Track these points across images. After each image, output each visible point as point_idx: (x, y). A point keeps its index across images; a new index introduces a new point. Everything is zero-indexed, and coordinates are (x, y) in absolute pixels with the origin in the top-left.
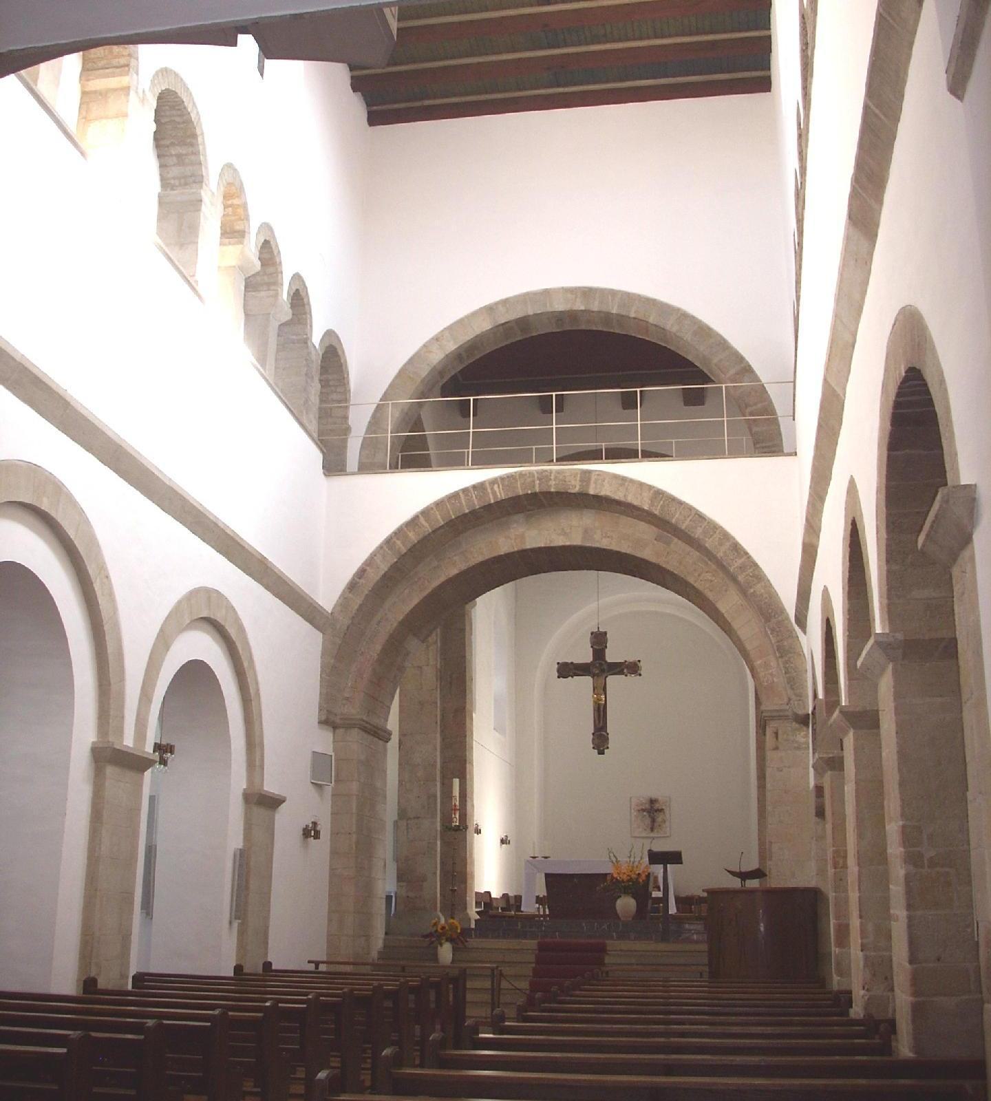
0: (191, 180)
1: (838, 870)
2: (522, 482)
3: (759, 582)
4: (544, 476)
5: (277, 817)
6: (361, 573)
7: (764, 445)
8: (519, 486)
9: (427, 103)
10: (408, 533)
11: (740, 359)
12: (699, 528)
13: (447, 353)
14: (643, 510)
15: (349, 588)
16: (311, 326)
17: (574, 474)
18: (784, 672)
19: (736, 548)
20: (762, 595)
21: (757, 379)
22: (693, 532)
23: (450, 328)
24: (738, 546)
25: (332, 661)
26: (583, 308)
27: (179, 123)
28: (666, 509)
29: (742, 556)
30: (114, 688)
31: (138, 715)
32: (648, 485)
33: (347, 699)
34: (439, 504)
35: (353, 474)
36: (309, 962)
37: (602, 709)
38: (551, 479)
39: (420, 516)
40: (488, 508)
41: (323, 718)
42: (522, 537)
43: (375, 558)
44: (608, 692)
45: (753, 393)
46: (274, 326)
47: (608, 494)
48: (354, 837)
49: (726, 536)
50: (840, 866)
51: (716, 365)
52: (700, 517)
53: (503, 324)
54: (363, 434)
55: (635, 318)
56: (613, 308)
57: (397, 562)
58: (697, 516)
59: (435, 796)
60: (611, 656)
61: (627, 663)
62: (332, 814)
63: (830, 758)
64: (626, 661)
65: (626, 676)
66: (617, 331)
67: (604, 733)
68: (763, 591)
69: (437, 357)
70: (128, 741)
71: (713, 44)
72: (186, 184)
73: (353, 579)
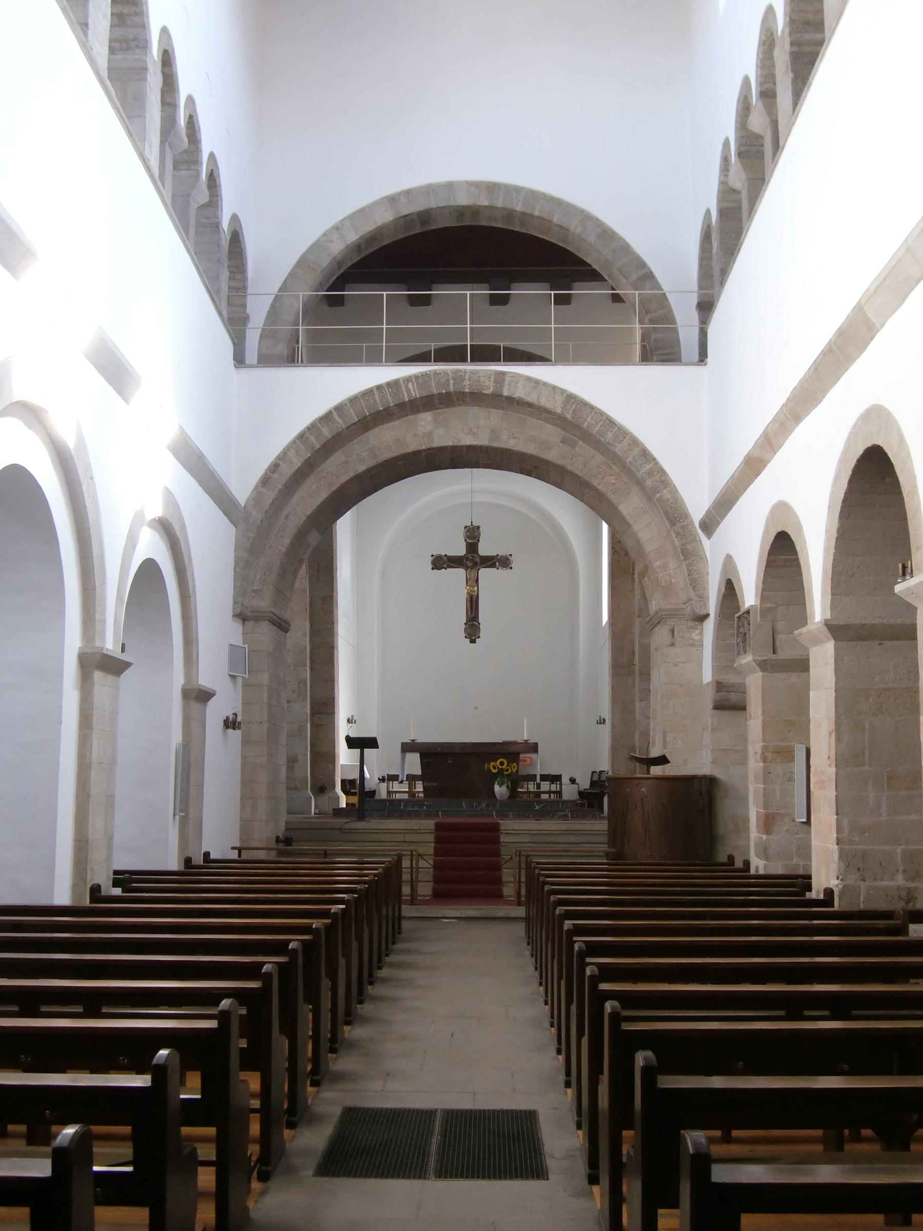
0: (133, 44)
1: (766, 764)
2: (436, 381)
7: (663, 352)
8: (433, 385)
10: (322, 429)
11: (642, 264)
12: (609, 433)
14: (555, 413)
16: (222, 210)
17: (488, 375)
18: (687, 574)
19: (645, 454)
20: (668, 500)
21: (659, 287)
23: (351, 217)
25: (246, 555)
26: (486, 203)
29: (650, 462)
31: (115, 617)
32: (561, 389)
33: (255, 591)
34: (353, 400)
36: (233, 848)
37: (474, 600)
38: (465, 379)
39: (333, 411)
41: (239, 610)
43: (288, 452)
44: (479, 585)
46: (194, 207)
47: (522, 396)
48: (265, 726)
49: (635, 442)
50: (769, 760)
51: (619, 270)
52: (611, 422)
53: (406, 216)
54: (261, 326)
55: (538, 217)
57: (310, 457)
59: (306, 681)
60: (484, 550)
61: (498, 557)
62: (242, 704)
63: (764, 660)
64: (498, 555)
65: (498, 569)
66: (516, 229)
67: (475, 623)
69: (338, 247)
72: (128, 48)
73: (266, 473)
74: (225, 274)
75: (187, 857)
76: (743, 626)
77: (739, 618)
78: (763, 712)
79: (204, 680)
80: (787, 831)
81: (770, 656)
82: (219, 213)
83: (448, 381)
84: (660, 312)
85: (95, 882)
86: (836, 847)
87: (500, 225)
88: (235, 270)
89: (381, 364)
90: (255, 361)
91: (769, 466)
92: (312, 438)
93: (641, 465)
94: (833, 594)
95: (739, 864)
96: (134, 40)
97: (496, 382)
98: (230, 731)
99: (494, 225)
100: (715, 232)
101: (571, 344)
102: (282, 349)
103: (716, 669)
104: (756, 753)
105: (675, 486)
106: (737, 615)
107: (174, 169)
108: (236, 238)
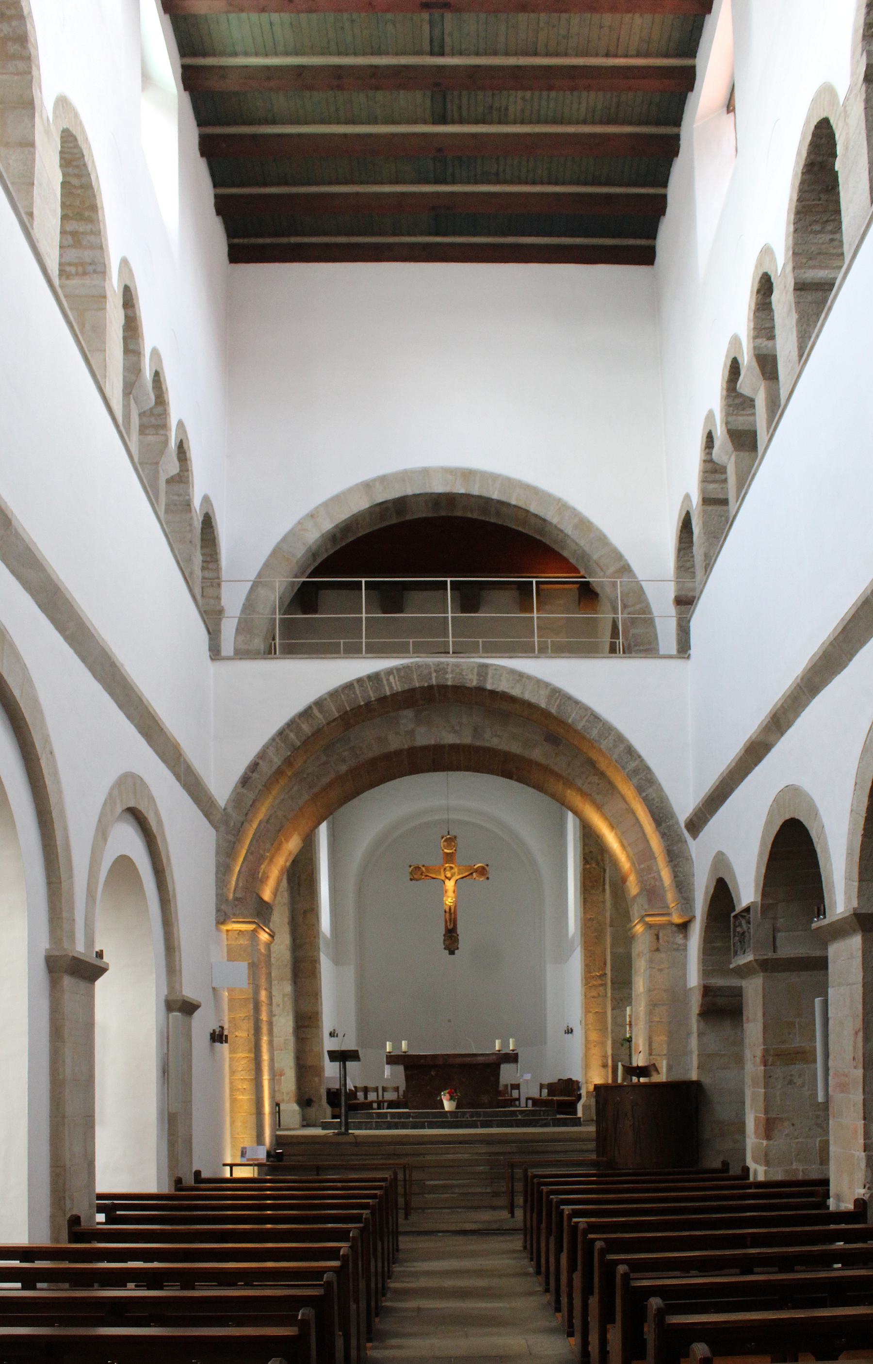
0: (91, 268)
1: (768, 1068)
2: (419, 673)
3: (651, 786)
4: (441, 670)
5: (193, 1021)
6: (254, 767)
7: (641, 648)
8: (415, 677)
9: (293, 240)
11: (619, 557)
13: (324, 532)
15: (241, 783)
16: (193, 487)
20: (653, 799)
21: (634, 576)
22: (588, 733)
23: (326, 505)
24: (632, 749)
26: (462, 491)
27: (75, 187)
28: (562, 708)
29: (636, 759)
34: (334, 694)
35: (228, 658)
40: (383, 700)
42: (412, 732)
43: (268, 750)
45: (631, 594)
52: (596, 718)
56: (494, 493)
58: (592, 716)
66: (493, 520)
68: (654, 795)
69: (313, 536)
70: (80, 948)
71: (609, 197)
72: (85, 274)
73: (246, 773)
74: (198, 558)
75: (178, 1177)
76: (740, 925)
77: (735, 917)
78: (764, 1014)
79: (189, 992)
80: (787, 1135)
81: (770, 955)
82: (191, 490)
83: (430, 674)
84: (638, 607)
85: (75, 1212)
86: (863, 1154)
87: (475, 516)
88: (208, 559)
89: (360, 655)
90: (231, 653)
91: (774, 751)
92: (292, 735)
93: (627, 763)
94: (861, 880)
95: (735, 1170)
96: (90, 264)
97: (479, 674)
98: (217, 1044)
99: (469, 515)
100: (696, 516)
101: (549, 640)
102: (258, 643)
103: (706, 971)
104: (754, 1057)
105: (660, 784)
106: (733, 914)
107: (140, 434)
108: (208, 523)
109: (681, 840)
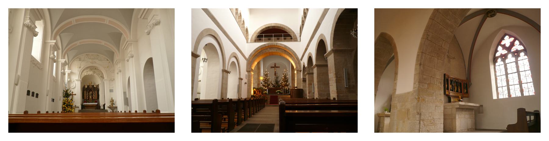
4: (272, 43)
6: (251, 54)
11: (293, 32)
30: (225, 62)
34: (260, 46)
42: (269, 51)
46: (241, 24)
60: (276, 66)
69: (259, 30)
70: (226, 69)
79: (242, 77)
103: (303, 76)
108: (247, 29)
109: (300, 62)
